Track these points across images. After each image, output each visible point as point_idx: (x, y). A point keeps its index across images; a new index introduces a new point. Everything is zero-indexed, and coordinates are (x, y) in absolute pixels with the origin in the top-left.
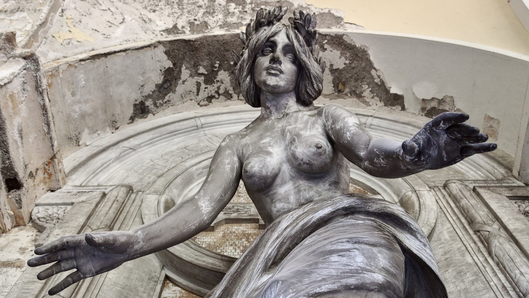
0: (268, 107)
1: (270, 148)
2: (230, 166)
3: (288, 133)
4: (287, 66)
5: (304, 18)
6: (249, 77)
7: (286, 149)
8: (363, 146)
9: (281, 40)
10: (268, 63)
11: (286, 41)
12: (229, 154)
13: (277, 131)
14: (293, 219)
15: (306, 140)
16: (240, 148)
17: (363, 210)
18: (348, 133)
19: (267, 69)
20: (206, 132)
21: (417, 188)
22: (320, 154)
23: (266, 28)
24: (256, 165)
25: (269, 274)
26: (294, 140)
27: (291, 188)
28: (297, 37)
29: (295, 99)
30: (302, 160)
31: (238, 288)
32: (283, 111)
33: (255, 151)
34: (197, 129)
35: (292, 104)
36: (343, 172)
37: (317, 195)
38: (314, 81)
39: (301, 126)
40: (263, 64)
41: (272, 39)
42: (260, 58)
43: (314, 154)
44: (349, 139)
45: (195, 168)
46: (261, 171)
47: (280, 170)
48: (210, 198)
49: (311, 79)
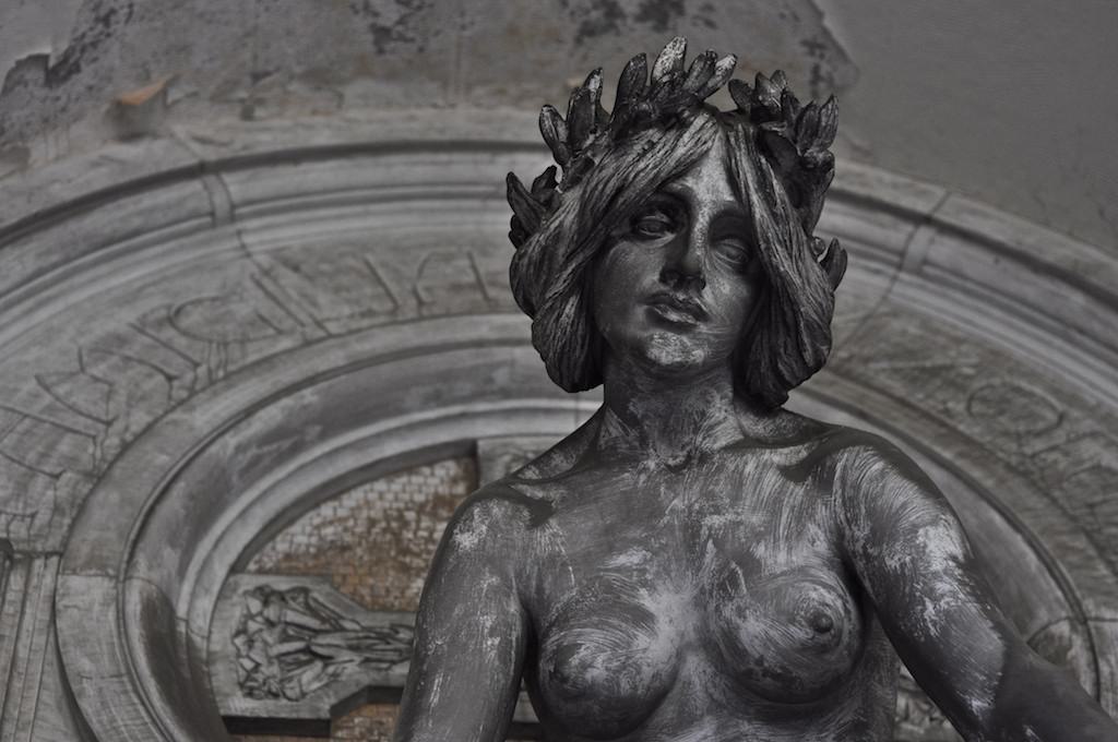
0: (633, 416)
1: (643, 591)
2: (497, 641)
3: (710, 545)
4: (721, 291)
6: (573, 301)
7: (699, 602)
9: (709, 188)
10: (656, 277)
11: (728, 197)
12: (494, 590)
13: (670, 527)
15: (778, 590)
16: (532, 570)
18: (930, 605)
19: (653, 300)
20: (248, 239)
21: (1089, 605)
22: (823, 649)
23: (653, 134)
26: (733, 579)
30: (760, 661)
32: (686, 439)
33: (591, 601)
34: (213, 225)
35: (720, 415)
36: (880, 681)
39: (756, 519)
40: (638, 278)
41: (677, 186)
42: (624, 245)
43: (804, 648)
44: (933, 631)
45: (231, 440)
46: (613, 681)
47: (674, 675)
49: (798, 333)
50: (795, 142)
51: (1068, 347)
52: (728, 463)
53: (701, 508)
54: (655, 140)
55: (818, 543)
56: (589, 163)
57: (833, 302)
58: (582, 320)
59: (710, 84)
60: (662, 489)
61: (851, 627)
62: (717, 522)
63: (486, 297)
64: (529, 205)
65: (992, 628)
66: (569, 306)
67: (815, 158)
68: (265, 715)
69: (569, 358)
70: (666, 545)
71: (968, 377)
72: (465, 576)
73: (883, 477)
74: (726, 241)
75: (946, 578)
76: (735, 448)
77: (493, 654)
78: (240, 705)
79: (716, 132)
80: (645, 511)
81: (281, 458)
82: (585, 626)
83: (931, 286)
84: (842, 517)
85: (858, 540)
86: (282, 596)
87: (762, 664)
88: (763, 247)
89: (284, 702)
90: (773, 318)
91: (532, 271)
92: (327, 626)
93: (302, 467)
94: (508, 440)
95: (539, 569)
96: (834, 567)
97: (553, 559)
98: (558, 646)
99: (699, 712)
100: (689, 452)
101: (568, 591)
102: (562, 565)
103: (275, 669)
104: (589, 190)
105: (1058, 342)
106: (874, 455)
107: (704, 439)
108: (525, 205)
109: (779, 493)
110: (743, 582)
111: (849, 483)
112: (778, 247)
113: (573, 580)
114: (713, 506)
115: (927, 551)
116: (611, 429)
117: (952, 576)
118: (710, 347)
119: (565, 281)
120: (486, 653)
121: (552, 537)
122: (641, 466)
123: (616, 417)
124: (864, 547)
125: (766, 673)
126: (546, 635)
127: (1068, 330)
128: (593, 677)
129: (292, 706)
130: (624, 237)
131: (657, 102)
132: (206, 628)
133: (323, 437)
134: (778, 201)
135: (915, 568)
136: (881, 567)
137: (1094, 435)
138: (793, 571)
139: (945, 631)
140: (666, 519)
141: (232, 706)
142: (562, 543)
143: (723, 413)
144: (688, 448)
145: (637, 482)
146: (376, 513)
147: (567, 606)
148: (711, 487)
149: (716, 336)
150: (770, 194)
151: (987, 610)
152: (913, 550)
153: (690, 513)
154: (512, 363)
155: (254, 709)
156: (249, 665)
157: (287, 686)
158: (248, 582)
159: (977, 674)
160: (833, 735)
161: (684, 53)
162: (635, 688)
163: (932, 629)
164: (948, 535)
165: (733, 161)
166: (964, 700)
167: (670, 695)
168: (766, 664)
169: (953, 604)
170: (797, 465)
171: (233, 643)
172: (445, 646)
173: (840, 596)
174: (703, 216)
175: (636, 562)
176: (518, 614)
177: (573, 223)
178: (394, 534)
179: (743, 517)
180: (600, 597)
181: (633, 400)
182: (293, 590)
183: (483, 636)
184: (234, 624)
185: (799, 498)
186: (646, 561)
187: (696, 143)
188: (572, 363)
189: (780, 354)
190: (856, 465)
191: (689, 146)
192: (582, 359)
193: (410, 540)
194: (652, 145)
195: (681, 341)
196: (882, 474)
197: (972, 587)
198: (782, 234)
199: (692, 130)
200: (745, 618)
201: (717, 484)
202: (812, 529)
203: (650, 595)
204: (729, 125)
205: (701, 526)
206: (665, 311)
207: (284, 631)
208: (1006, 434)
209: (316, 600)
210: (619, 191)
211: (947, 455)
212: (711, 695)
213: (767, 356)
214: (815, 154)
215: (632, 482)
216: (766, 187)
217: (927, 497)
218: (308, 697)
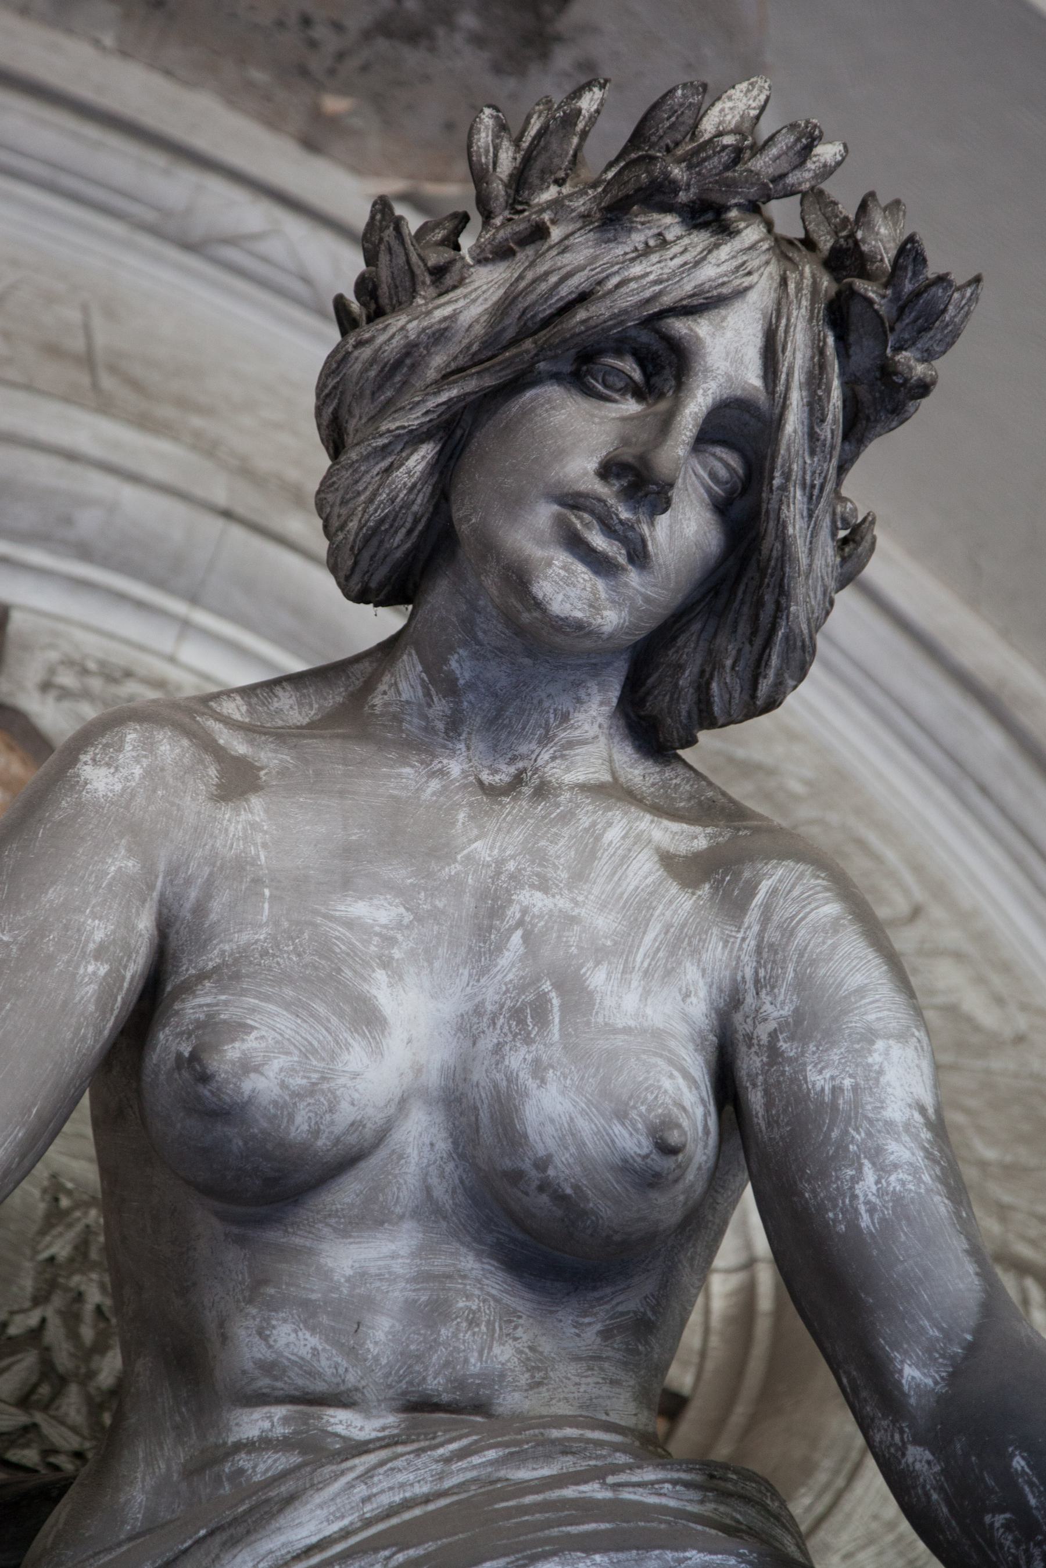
1: (380, 975)
2: (103, 969)
3: (516, 938)
4: (685, 531)
5: (908, 287)
7: (468, 1027)
8: (934, 1332)
9: (727, 353)
10: (592, 465)
11: (753, 378)
18: (870, 1175)
19: (573, 501)
23: (670, 224)
24: (277, 1063)
26: (540, 1009)
27: (399, 1267)
28: (816, 379)
29: (614, 695)
37: (524, 1379)
38: (775, 661)
39: (605, 923)
40: (560, 455)
41: (679, 326)
42: (553, 391)
47: (382, 1135)
49: (768, 643)
50: (892, 329)
51: (954, 807)
52: (580, 814)
54: (670, 236)
55: (693, 999)
56: (539, 232)
57: (828, 613)
58: (428, 489)
59: (791, 179)
60: (461, 816)
61: (704, 1158)
62: (540, 904)
63: (95, 386)
64: (408, 262)
65: (966, 1251)
66: (415, 457)
67: (910, 368)
69: (382, 542)
70: (443, 912)
71: (796, 798)
72: (82, 839)
73: (836, 932)
74: (719, 450)
75: (906, 1138)
77: (91, 989)
79: (767, 263)
82: (267, 998)
84: (749, 972)
85: (765, 1020)
87: (544, 1169)
88: (777, 482)
90: (736, 605)
91: (372, 373)
94: (61, 627)
95: (211, 874)
96: (703, 1049)
97: (240, 865)
98: (210, 1016)
99: (398, 1210)
101: (247, 927)
102: (253, 881)
104: (530, 276)
105: (941, 793)
106: (826, 889)
107: (553, 758)
108: (401, 260)
109: (651, 894)
110: (557, 1020)
111: (776, 918)
113: (266, 912)
114: (538, 875)
115: (883, 1080)
116: (403, 686)
117: (916, 1137)
118: (630, 613)
119: (427, 413)
121: (249, 828)
122: (436, 766)
123: (419, 668)
124: (773, 1035)
126: (187, 989)
127: (960, 777)
128: (253, 1091)
130: (556, 377)
131: (699, 174)
134: (830, 417)
135: (856, 1104)
136: (793, 1080)
137: (958, 956)
138: (644, 1031)
140: (455, 868)
143: (596, 726)
144: (520, 765)
147: (243, 955)
148: (543, 843)
149: (647, 599)
150: (820, 398)
151: (961, 1217)
152: (860, 1071)
153: (498, 873)
154: (112, 508)
160: (599, 1327)
161: (763, 109)
162: (316, 1133)
164: (918, 1066)
166: (891, 1360)
167: (363, 1164)
168: (551, 1172)
170: (685, 857)
172: (15, 949)
174: (704, 395)
176: (147, 936)
177: (477, 321)
181: (461, 651)
183: (83, 952)
185: (682, 913)
186: (400, 926)
187: (737, 268)
188: (381, 553)
189: (724, 667)
190: (795, 893)
192: (399, 554)
194: (664, 243)
195: (594, 585)
196: (835, 926)
197: (942, 1168)
198: (814, 473)
200: (543, 1081)
202: (691, 973)
204: (789, 259)
205: (510, 902)
210: (583, 298)
213: (699, 662)
214: (911, 363)
216: (819, 387)
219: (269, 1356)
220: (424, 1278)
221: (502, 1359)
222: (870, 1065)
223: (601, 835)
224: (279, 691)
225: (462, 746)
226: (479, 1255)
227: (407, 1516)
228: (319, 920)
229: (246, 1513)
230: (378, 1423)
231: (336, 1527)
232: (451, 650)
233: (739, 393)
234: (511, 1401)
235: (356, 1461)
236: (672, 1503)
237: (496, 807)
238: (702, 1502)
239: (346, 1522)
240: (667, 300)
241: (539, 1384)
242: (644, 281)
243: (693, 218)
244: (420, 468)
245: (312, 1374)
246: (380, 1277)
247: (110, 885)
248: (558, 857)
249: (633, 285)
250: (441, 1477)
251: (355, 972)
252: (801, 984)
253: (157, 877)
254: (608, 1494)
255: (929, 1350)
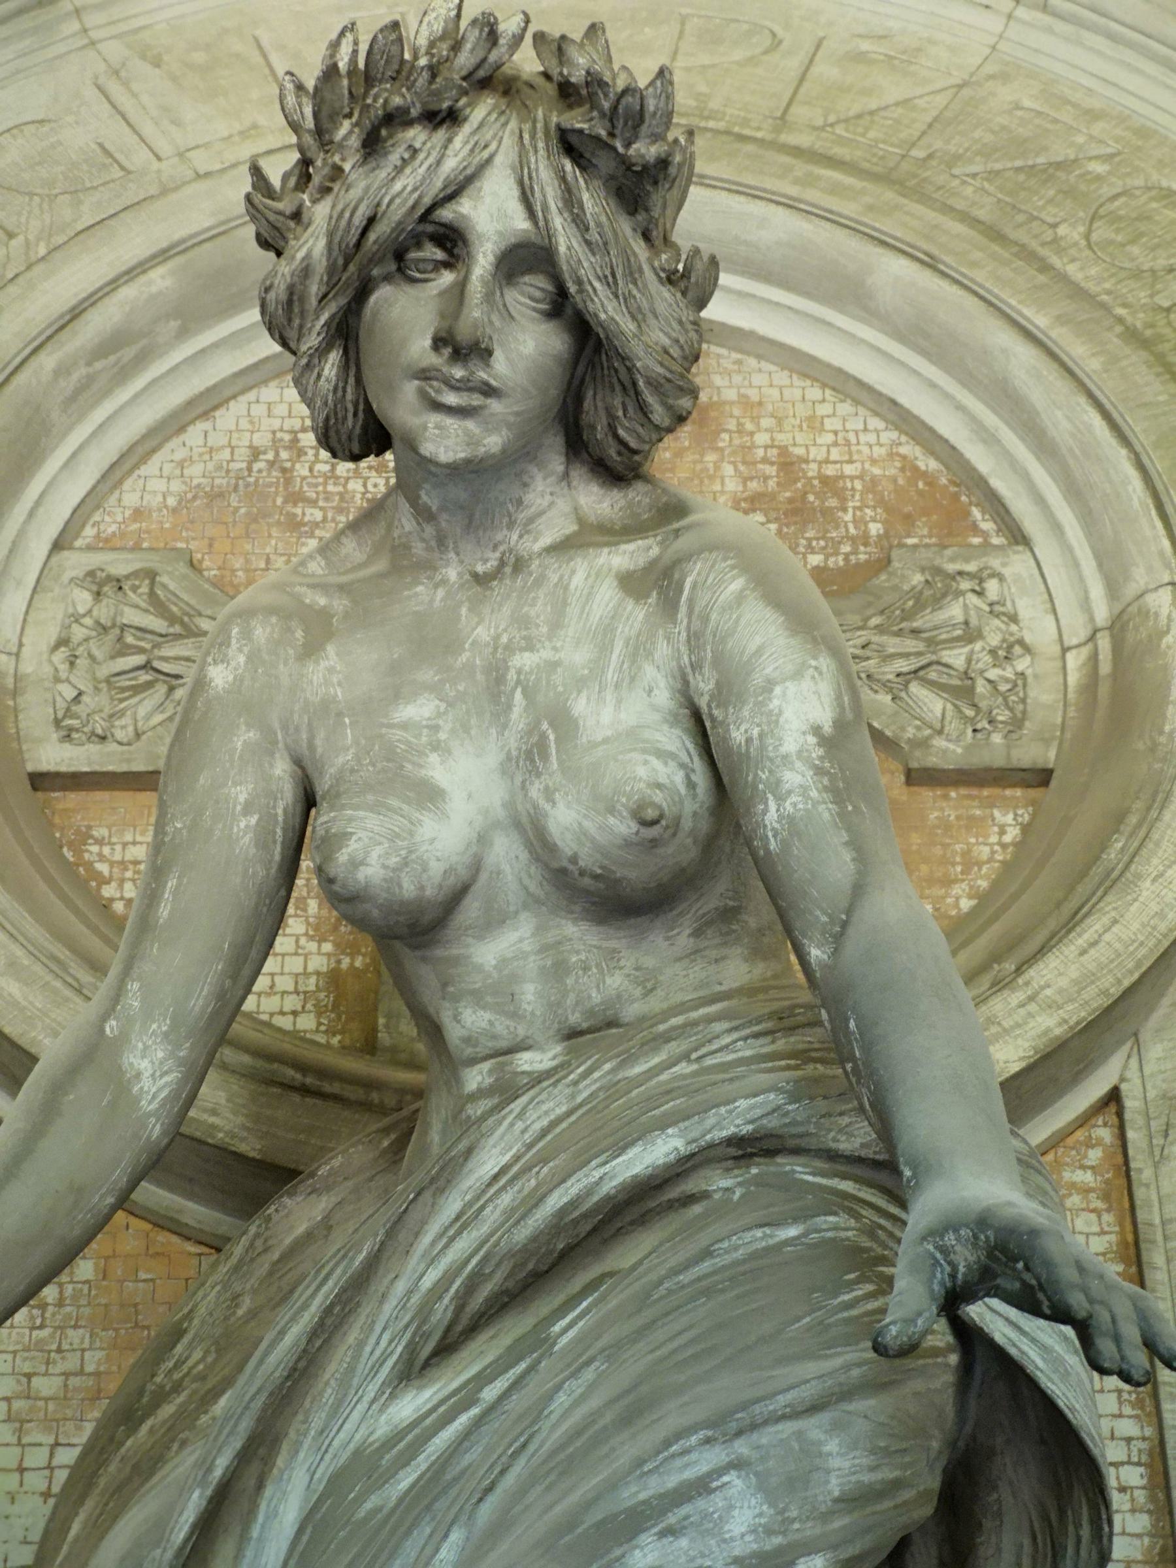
1: (434, 758)
2: (253, 820)
3: (518, 695)
5: (606, 105)
6: (334, 357)
7: (507, 767)
9: (492, 215)
10: (428, 342)
11: (522, 224)
14: (528, 1137)
17: (813, 1144)
19: (424, 375)
23: (416, 135)
25: (421, 1388)
26: (542, 745)
27: (527, 946)
28: (570, 200)
30: (574, 859)
31: (300, 1417)
37: (638, 992)
43: (628, 844)
44: (773, 845)
45: (48, 361)
47: (476, 866)
48: (174, 1027)
53: (510, 640)
54: (417, 145)
55: (656, 692)
60: (464, 611)
68: (86, 769)
69: (337, 432)
73: (739, 604)
74: (527, 279)
76: (563, 547)
78: (53, 756)
80: (433, 643)
81: (123, 375)
82: (357, 808)
83: (1061, 27)
86: (118, 584)
89: (114, 747)
92: (177, 629)
93: (154, 382)
97: (326, 704)
99: (512, 908)
100: (503, 554)
101: (338, 759)
103: (103, 700)
106: (733, 567)
107: (521, 537)
111: (697, 610)
112: (597, 285)
114: (524, 638)
115: (782, 720)
118: (509, 429)
120: (238, 840)
122: (438, 578)
125: (582, 873)
129: (122, 753)
130: (387, 278)
132: (15, 640)
133: (183, 333)
134: (592, 224)
135: (763, 747)
139: (786, 845)
140: (464, 657)
141: (43, 758)
142: (340, 684)
145: (432, 601)
146: (261, 439)
147: (339, 779)
148: (526, 609)
149: (517, 414)
153: (496, 649)
155: (71, 759)
156: (70, 693)
157: (117, 723)
158: (75, 562)
159: (818, 913)
160: (688, 932)
163: (772, 840)
165: (526, 171)
168: (581, 863)
169: (801, 806)
170: (644, 569)
171: (50, 661)
172: (185, 832)
173: (682, 766)
175: (427, 715)
176: (287, 777)
178: (284, 470)
179: (562, 655)
180: (379, 766)
182: (135, 574)
184: (52, 633)
185: (637, 626)
186: (439, 715)
187: (472, 150)
191: (461, 155)
192: (358, 431)
193: (304, 478)
194: (415, 152)
196: (740, 598)
199: (467, 129)
200: (554, 803)
201: (533, 605)
202: (650, 672)
203: (442, 762)
205: (507, 668)
206: (438, 391)
207: (120, 639)
208: (1137, 274)
209: (165, 587)
210: (371, 221)
211: (1040, 320)
212: (526, 888)
215: (427, 599)
217: (794, 633)
218: (144, 737)
219: (464, 1033)
220: (544, 949)
221: (615, 986)
222: (771, 711)
223: (568, 584)
224: (344, 540)
225: (452, 555)
226: (575, 921)
227: (558, 1130)
228: (384, 730)
229: (438, 1173)
230: (550, 1054)
231: (507, 1157)
232: (419, 487)
233: (513, 240)
234: (631, 1011)
235: (512, 1106)
236: (748, 1053)
237: (488, 593)
238: (773, 1042)
239: (514, 1150)
240: (427, 201)
241: (652, 990)
242: (405, 194)
243: (430, 121)
244: (334, 373)
245: (494, 1037)
246: (516, 958)
247: (241, 758)
248: (538, 616)
249: (398, 201)
250: (573, 1096)
251: (414, 763)
252: (717, 662)
253: (275, 734)
254: (695, 1067)
255: (823, 934)
